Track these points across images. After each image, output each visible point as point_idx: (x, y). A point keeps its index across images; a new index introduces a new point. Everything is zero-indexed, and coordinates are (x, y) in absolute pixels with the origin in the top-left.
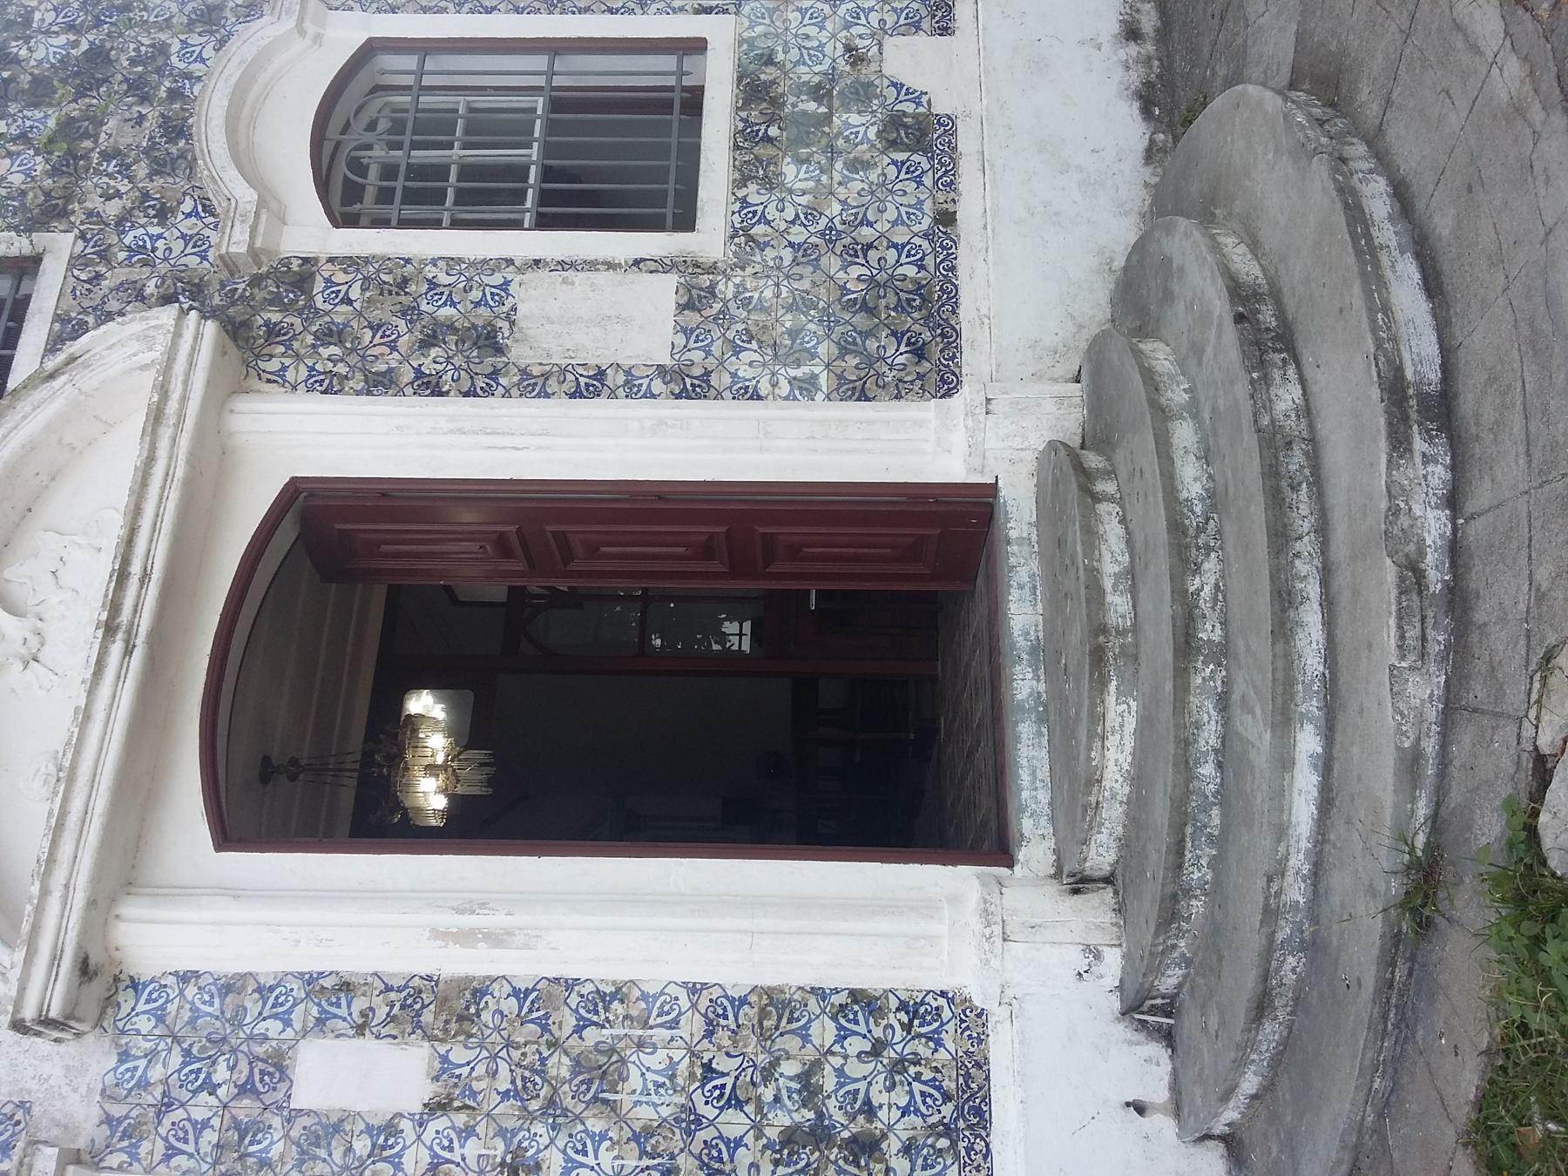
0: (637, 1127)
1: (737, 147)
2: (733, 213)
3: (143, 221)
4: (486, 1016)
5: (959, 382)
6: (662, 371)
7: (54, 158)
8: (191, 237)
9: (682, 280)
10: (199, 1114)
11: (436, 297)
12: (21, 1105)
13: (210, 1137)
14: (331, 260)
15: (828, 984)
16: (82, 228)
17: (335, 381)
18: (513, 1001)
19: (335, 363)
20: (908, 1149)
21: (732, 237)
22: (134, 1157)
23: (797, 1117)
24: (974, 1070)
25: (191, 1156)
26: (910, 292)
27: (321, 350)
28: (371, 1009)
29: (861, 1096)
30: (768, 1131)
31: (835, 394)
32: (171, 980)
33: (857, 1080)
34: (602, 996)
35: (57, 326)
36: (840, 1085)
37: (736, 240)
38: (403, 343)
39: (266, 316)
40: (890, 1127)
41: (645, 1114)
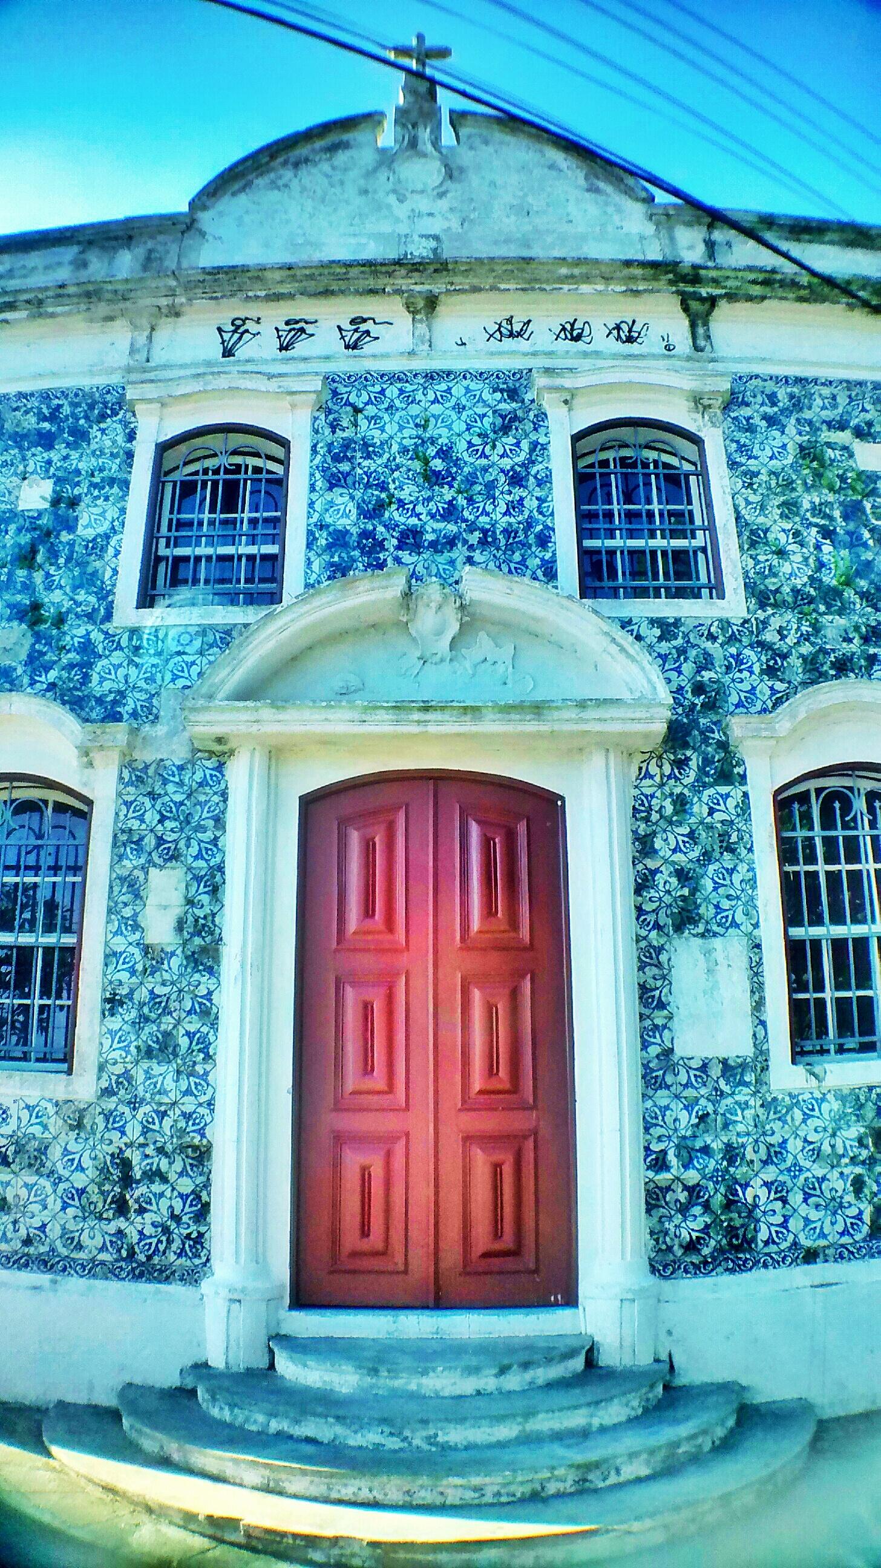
0: (133, 1072)
1: (871, 1089)
2: (811, 1093)
3: (764, 659)
4: (197, 976)
5: (665, 1278)
6: (668, 1052)
7: (808, 589)
8: (754, 694)
9: (749, 1060)
10: (148, 817)
11: (721, 876)
12: (157, 717)
13: (135, 824)
14: (746, 795)
15: (213, 1189)
16: (753, 620)
17: (643, 815)
18: (205, 992)
19: (659, 811)
20: (120, 1233)
21: (790, 1095)
22: (127, 785)
23: (136, 1169)
24: (164, 1275)
25: (126, 816)
26: (744, 1235)
27: (669, 800)
28: (202, 906)
29: (148, 1207)
30: (129, 1151)
31: (652, 1185)
32: (223, 786)
33: (157, 1204)
34: (207, 1048)
35: (671, 621)
36: (155, 1195)
37: (787, 1098)
38: (679, 857)
39: (694, 757)
40: (132, 1223)
41: (140, 1077)
